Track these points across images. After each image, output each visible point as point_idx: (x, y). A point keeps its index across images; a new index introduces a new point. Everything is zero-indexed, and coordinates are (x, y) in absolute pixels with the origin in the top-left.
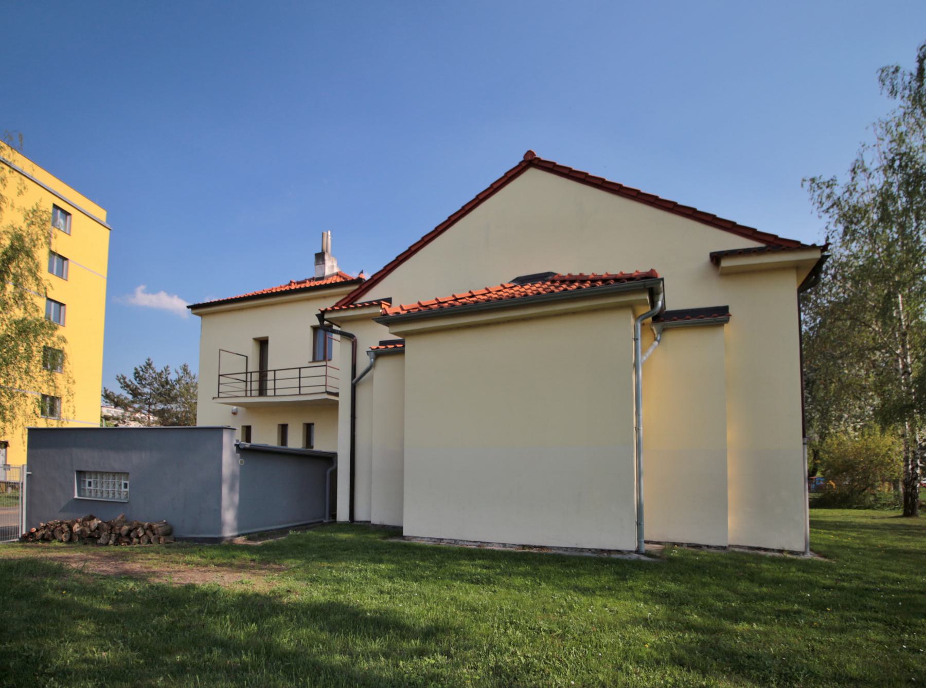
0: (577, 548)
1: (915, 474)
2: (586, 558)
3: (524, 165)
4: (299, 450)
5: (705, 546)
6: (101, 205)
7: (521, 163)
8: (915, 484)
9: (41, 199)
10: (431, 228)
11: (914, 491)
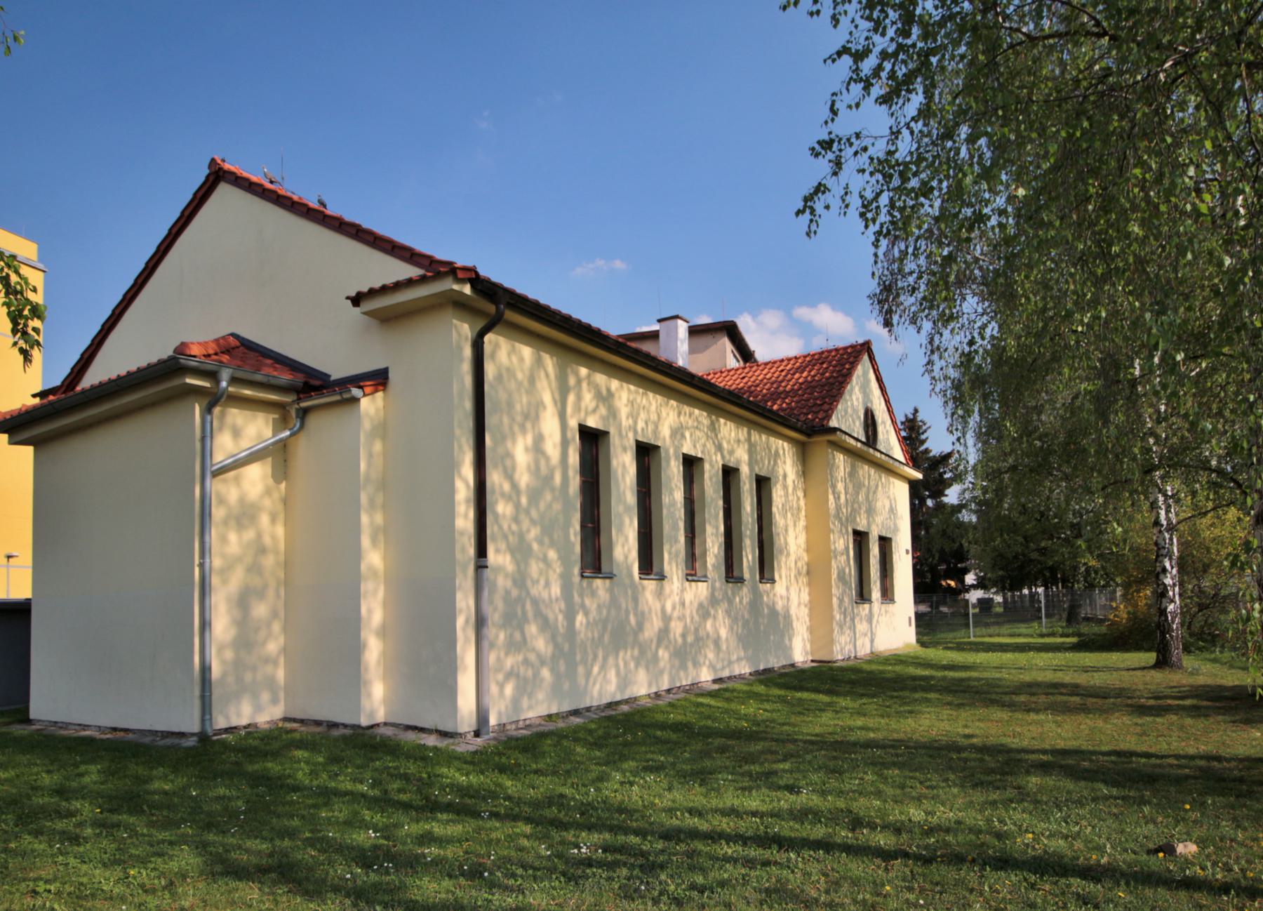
0: (149, 731)
1: (1162, 587)
2: (91, 740)
3: (211, 179)
4: (898, 659)
5: (343, 724)
6: (29, 236)
7: (208, 177)
8: (1163, 606)
9: (835, 26)
10: (140, 266)
11: (1163, 618)
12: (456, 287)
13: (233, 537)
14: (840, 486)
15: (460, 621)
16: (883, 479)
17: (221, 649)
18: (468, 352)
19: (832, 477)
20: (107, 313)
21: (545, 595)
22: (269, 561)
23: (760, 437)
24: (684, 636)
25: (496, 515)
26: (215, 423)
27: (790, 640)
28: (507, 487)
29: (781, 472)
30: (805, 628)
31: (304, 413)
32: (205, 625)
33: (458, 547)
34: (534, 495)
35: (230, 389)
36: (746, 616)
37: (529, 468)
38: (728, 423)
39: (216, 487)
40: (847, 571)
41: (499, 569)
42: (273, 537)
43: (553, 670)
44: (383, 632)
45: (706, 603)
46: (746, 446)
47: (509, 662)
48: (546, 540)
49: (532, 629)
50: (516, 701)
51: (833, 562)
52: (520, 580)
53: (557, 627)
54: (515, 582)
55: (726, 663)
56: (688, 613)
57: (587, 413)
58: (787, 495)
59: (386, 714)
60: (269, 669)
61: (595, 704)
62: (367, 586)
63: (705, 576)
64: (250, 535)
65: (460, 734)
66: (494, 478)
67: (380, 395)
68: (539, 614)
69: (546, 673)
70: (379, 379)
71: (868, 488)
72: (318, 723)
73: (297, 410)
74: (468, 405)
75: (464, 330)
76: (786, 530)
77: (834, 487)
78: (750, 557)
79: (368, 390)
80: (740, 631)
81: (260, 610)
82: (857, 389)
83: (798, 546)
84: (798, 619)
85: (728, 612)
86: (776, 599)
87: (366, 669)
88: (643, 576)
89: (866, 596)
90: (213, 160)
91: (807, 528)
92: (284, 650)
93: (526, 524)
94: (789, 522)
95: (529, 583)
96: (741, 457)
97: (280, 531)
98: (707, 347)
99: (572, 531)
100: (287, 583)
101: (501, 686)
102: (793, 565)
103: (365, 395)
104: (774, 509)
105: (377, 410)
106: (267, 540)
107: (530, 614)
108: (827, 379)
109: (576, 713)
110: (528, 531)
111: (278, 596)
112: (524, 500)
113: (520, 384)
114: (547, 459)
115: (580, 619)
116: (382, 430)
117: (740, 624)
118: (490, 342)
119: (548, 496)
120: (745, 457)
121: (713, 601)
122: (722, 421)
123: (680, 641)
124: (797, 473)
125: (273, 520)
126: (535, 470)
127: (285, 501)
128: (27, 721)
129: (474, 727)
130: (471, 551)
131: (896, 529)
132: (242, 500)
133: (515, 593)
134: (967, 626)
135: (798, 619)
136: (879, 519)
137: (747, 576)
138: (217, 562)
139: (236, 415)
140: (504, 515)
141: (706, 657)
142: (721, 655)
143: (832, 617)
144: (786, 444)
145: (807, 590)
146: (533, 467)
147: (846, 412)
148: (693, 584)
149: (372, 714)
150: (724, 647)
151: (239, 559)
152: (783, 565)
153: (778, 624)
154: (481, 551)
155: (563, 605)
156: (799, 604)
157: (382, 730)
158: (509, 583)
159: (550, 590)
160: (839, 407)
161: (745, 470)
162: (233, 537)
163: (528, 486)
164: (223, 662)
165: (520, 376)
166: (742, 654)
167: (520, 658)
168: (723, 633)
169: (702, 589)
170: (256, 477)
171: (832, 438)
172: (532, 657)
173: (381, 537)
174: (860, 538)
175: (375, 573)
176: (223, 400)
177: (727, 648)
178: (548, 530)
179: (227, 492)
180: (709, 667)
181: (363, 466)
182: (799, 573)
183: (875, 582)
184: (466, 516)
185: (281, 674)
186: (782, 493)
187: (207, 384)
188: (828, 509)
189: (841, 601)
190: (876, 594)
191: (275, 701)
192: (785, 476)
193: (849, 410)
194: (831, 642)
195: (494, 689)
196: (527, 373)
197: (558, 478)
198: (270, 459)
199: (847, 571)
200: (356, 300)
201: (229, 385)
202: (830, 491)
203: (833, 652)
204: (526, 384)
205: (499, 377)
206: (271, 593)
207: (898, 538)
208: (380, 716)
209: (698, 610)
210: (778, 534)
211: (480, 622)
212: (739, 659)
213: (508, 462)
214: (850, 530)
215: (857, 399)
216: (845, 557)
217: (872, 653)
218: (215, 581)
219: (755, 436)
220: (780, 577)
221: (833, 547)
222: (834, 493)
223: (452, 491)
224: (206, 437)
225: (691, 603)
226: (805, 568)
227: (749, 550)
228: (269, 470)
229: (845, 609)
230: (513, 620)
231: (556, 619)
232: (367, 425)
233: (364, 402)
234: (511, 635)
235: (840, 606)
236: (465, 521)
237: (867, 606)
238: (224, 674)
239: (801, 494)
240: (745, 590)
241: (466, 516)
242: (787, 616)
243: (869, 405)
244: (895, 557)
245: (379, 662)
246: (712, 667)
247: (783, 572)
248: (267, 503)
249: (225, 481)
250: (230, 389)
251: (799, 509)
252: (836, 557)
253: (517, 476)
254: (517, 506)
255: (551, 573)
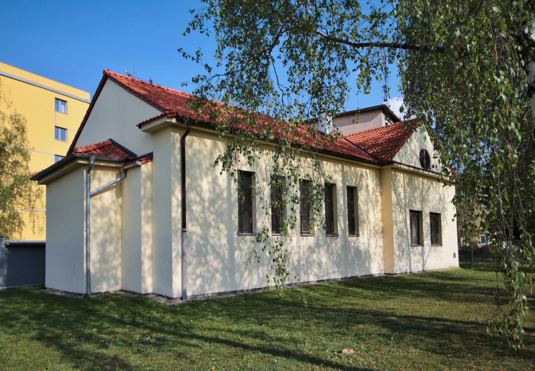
12: (168, 120)
13: (99, 220)
14: (401, 190)
15: (174, 254)
16: (434, 184)
17: (94, 263)
18: (178, 145)
19: (394, 185)
20: (75, 133)
21: (218, 243)
22: (113, 230)
23: (350, 168)
24: (299, 261)
25: (192, 211)
26: (91, 177)
27: (369, 264)
28: (198, 199)
29: (365, 184)
30: (380, 258)
31: (126, 171)
32: (88, 255)
33: (173, 224)
34: (213, 202)
35: (95, 163)
36: (339, 252)
37: (209, 191)
38: (329, 163)
39: (92, 201)
40: (405, 230)
41: (192, 233)
42: (116, 220)
43: (223, 275)
44: (151, 258)
45: (313, 246)
46: (341, 173)
47: (198, 271)
48: (219, 220)
49: (211, 257)
50: (202, 287)
51: (394, 227)
52: (205, 237)
53: (224, 257)
54: (202, 238)
55: (325, 274)
56: (302, 250)
57: (242, 165)
58: (368, 195)
59: (154, 289)
60: (114, 271)
61: (245, 289)
62: (144, 240)
63: (314, 234)
64: (106, 219)
65: (174, 299)
66: (191, 196)
67: (149, 163)
68: (214, 251)
69: (218, 276)
70: (149, 157)
71: (422, 190)
72: (130, 292)
73: (124, 170)
74: (178, 167)
75: (177, 136)
76: (368, 212)
77: (396, 191)
78: (342, 225)
79: (143, 162)
80: (335, 259)
81: (110, 249)
82: (415, 141)
83: (376, 219)
84: (375, 254)
85: (327, 251)
86: (360, 245)
87: (144, 272)
88: (274, 234)
89: (421, 243)
90: (104, 71)
91: (382, 211)
92: (121, 264)
93: (207, 214)
94: (369, 208)
95: (210, 239)
96: (338, 179)
97: (119, 217)
98: (372, 119)
99: (233, 216)
100: (122, 238)
101: (195, 280)
102: (372, 228)
103: (143, 164)
104: (359, 202)
105: (148, 170)
106: (113, 221)
107: (210, 251)
108: (398, 136)
109: (234, 292)
110: (209, 217)
111: (117, 243)
112: (207, 204)
113: (205, 156)
114: (220, 186)
115: (237, 254)
116: (151, 178)
117: (335, 256)
118: (189, 140)
119: (220, 202)
120: (340, 178)
121: (318, 245)
122: (325, 162)
123: (296, 263)
124: (376, 184)
125: (116, 213)
126: (213, 191)
127: (121, 206)
128: (45, 288)
129: (180, 296)
130: (180, 226)
131: (444, 209)
132: (102, 207)
133: (202, 242)
134: (471, 258)
135: (375, 254)
136: (430, 205)
137: (340, 233)
138: (92, 230)
139: (100, 173)
140: (196, 211)
141: (312, 270)
142: (322, 270)
143: (393, 253)
144: (368, 171)
145: (382, 240)
146: (212, 190)
147: (406, 153)
148: (305, 237)
149: (146, 290)
150: (324, 266)
151: (101, 228)
152: (365, 227)
153: (362, 256)
154: (184, 225)
155: (227, 247)
156: (376, 247)
157: (150, 296)
158: (199, 239)
159: (220, 241)
160: (401, 151)
161: (339, 185)
162: (99, 220)
163: (209, 198)
164: (95, 268)
165: (205, 153)
166: (336, 270)
167: (205, 269)
168: (324, 260)
169: (310, 240)
170: (108, 197)
171: (392, 166)
172: (211, 269)
173: (151, 220)
174: (416, 216)
175: (147, 234)
176: (93, 168)
177: (326, 267)
178: (219, 215)
179: (96, 203)
180: (314, 275)
181: (142, 192)
182: (377, 232)
183: (427, 236)
184: (177, 212)
185: (119, 274)
186: (365, 194)
187: (87, 163)
188: (391, 201)
189: (400, 245)
190: (427, 241)
191: (116, 283)
192: (367, 186)
193: (408, 152)
194: (393, 265)
195: (190, 282)
196: (209, 151)
197: (225, 194)
198: (115, 189)
199: (405, 230)
200: (140, 126)
201: (94, 162)
202: (393, 192)
203: (394, 270)
204: (208, 156)
205: (194, 154)
206: (115, 241)
207: (446, 214)
208: (150, 290)
209: (307, 250)
210: (362, 214)
211: (183, 255)
212: (333, 272)
213: (199, 189)
214: (408, 211)
215: (415, 146)
216: (403, 224)
217: (423, 271)
218: (91, 237)
219: (346, 168)
220: (363, 234)
221: (394, 219)
222: (395, 193)
223: (170, 202)
224: (89, 182)
225: (304, 246)
226: (381, 229)
227: (341, 222)
228: (114, 194)
229: (403, 249)
230: (201, 253)
231: (224, 254)
232: (144, 176)
233: (143, 167)
234: (200, 260)
235: (399, 248)
236: (176, 213)
237: (420, 248)
238: (96, 273)
239: (378, 194)
240: (339, 240)
241: (177, 212)
242: (367, 252)
243: (424, 148)
244: (443, 223)
245: (149, 270)
246: (316, 275)
247: (365, 232)
248: (113, 207)
249: (95, 199)
250: (95, 163)
251: (377, 201)
252: (396, 224)
253: (203, 195)
254: (204, 207)
255: (221, 234)
